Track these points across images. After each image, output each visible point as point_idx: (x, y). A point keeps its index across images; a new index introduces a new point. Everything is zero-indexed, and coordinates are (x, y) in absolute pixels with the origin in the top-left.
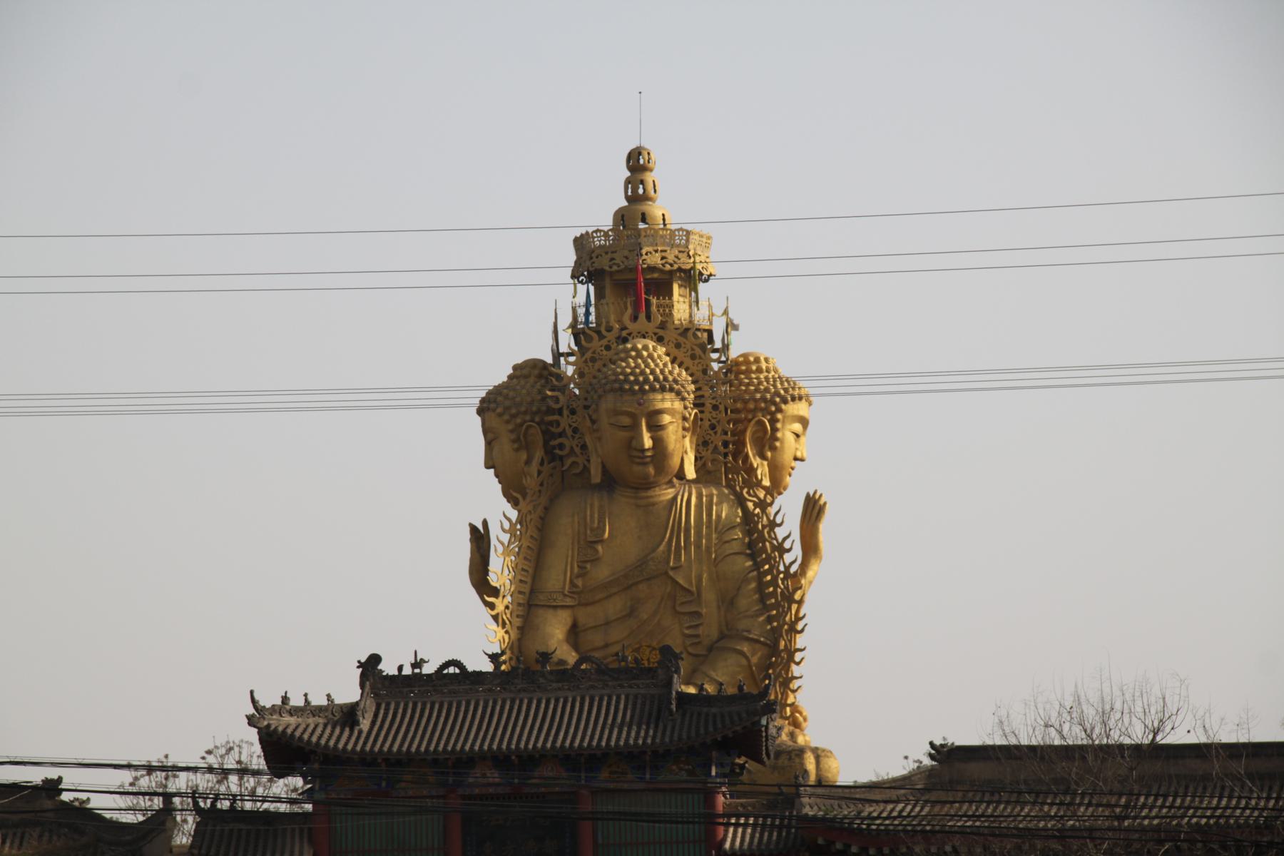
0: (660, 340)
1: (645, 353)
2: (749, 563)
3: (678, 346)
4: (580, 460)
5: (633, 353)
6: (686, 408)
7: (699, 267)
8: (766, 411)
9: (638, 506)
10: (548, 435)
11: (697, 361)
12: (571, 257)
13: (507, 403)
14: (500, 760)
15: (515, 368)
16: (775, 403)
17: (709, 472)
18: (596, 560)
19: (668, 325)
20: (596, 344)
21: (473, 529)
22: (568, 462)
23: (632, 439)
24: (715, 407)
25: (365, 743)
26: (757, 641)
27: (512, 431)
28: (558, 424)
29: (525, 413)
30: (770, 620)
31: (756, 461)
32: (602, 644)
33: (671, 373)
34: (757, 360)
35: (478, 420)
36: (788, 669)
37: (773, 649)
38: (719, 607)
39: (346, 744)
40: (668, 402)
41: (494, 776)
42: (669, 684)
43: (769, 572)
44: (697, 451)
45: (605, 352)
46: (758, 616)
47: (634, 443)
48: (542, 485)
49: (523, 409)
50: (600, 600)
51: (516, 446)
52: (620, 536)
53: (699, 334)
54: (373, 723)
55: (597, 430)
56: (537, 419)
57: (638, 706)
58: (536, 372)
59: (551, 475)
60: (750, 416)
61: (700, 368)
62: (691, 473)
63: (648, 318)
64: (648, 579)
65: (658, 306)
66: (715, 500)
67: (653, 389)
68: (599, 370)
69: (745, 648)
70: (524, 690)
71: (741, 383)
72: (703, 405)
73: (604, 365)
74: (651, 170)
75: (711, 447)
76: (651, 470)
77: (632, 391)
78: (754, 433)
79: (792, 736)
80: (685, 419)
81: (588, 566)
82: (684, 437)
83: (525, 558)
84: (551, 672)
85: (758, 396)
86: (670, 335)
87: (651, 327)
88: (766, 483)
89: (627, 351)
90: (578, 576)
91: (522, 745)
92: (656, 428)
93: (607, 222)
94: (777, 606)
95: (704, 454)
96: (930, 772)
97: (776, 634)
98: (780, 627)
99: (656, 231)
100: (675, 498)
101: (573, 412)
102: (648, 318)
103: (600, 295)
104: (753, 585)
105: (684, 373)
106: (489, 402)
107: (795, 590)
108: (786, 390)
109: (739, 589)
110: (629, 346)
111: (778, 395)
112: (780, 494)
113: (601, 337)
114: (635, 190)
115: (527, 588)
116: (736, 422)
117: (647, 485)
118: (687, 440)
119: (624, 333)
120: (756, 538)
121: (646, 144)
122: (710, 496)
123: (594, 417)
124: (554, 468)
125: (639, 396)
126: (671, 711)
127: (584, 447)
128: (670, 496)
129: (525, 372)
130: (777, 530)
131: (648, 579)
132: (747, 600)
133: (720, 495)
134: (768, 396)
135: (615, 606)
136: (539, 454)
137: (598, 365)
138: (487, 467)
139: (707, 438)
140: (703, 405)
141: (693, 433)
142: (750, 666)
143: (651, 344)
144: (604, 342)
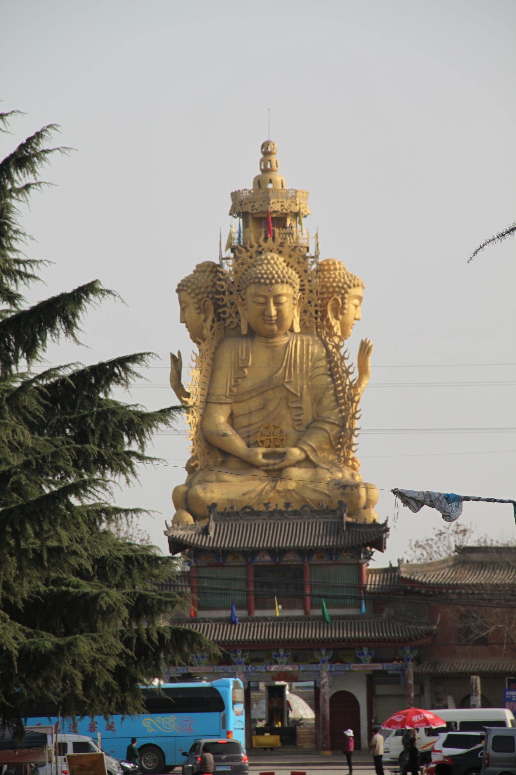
0: (280, 253)
1: (272, 262)
2: (330, 379)
3: (290, 256)
4: (235, 320)
5: (266, 262)
6: (295, 292)
7: (302, 211)
8: (339, 293)
9: (268, 347)
10: (217, 306)
11: (301, 265)
12: (229, 203)
13: (194, 287)
14: (271, 551)
15: (198, 266)
16: (343, 288)
17: (307, 328)
18: (244, 377)
19: (285, 245)
20: (245, 255)
21: (173, 357)
22: (228, 321)
23: (264, 310)
24: (311, 291)
25: (213, 543)
26: (333, 424)
27: (196, 303)
28: (223, 300)
29: (204, 293)
30: (341, 411)
31: (333, 322)
32: (247, 424)
33: (287, 273)
34: (334, 263)
35: (177, 295)
36: (350, 439)
37: (343, 427)
38: (312, 404)
39: (205, 543)
40: (284, 289)
41: (268, 558)
42: (342, 517)
43: (341, 384)
44: (301, 316)
45: (249, 260)
46: (334, 409)
47: (266, 313)
48: (213, 334)
49: (202, 290)
50: (246, 400)
51: (198, 311)
52: (257, 361)
53: (302, 249)
54: (215, 533)
55: (245, 305)
56: (210, 296)
57: (329, 527)
58: (210, 269)
59: (219, 329)
60: (330, 296)
61: (303, 269)
62: (297, 328)
63: (274, 239)
64: (273, 388)
65: (279, 234)
66: (311, 343)
67: (277, 282)
68: (246, 270)
69: (327, 427)
70: (279, 519)
71: (325, 277)
72: (304, 290)
73: (249, 267)
74: (274, 154)
75: (308, 314)
76: (275, 327)
77: (265, 284)
78: (332, 305)
79: (353, 476)
80: (294, 299)
81: (240, 380)
82: (294, 309)
83: (205, 376)
84: (291, 512)
85: (335, 284)
86: (286, 250)
87: (275, 246)
88: (339, 334)
89: (262, 260)
90: (234, 386)
91: (280, 545)
92: (278, 304)
93: (250, 186)
94: (345, 404)
95: (304, 317)
96: (456, 558)
97: (344, 420)
98: (347, 416)
99: (278, 191)
100: (288, 343)
101: (231, 293)
102: (274, 239)
103: (246, 225)
104: (332, 392)
105: (294, 273)
106: (183, 286)
107: (355, 395)
108: (350, 281)
109: (324, 394)
110: (263, 257)
111: (345, 283)
112: (346, 339)
113: (247, 251)
114: (265, 165)
115: (205, 393)
116: (322, 300)
117: (272, 335)
118: (295, 310)
119: (260, 249)
120: (333, 367)
121: (272, 139)
122: (308, 341)
123: (244, 297)
124: (220, 325)
125: (269, 286)
126: (343, 531)
127: (237, 313)
128: (286, 342)
129: (203, 269)
130: (345, 361)
131: (273, 388)
132: (328, 400)
133: (313, 341)
134: (340, 285)
135: (254, 403)
136: (211, 316)
137: (245, 267)
138: (182, 322)
139: (306, 308)
140: (304, 290)
141: (299, 305)
142: (330, 438)
143: (276, 256)
144: (249, 254)
